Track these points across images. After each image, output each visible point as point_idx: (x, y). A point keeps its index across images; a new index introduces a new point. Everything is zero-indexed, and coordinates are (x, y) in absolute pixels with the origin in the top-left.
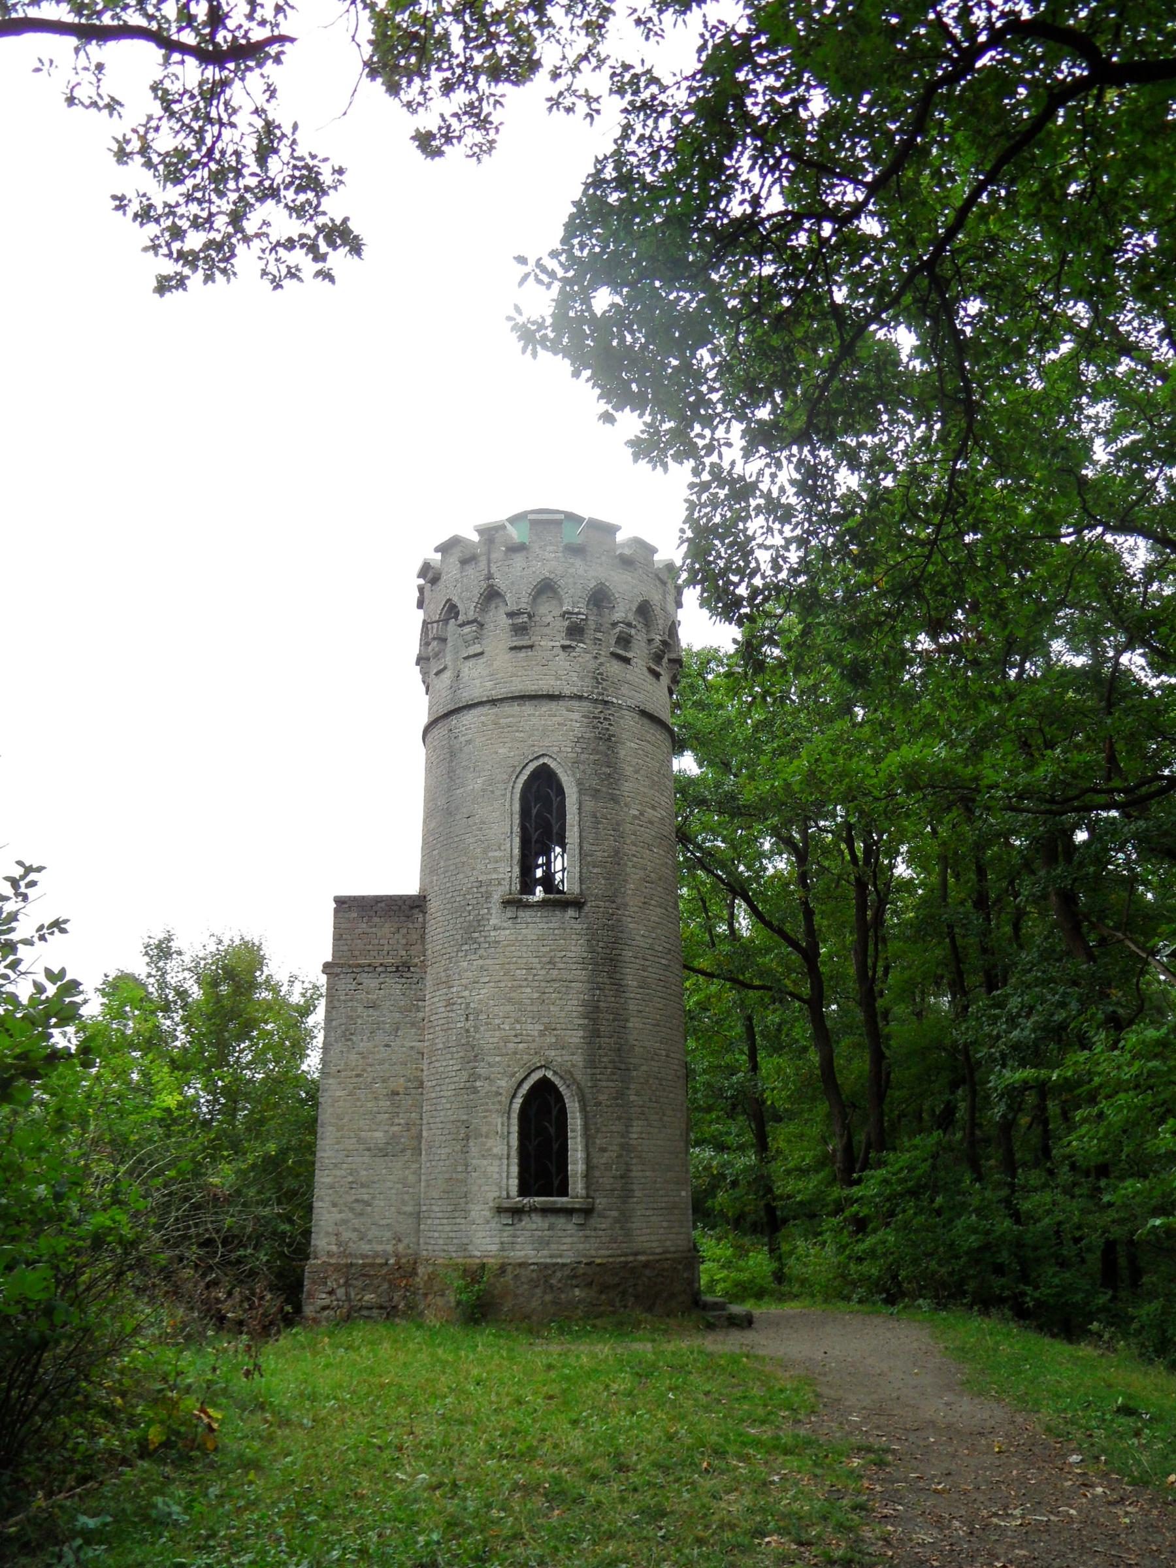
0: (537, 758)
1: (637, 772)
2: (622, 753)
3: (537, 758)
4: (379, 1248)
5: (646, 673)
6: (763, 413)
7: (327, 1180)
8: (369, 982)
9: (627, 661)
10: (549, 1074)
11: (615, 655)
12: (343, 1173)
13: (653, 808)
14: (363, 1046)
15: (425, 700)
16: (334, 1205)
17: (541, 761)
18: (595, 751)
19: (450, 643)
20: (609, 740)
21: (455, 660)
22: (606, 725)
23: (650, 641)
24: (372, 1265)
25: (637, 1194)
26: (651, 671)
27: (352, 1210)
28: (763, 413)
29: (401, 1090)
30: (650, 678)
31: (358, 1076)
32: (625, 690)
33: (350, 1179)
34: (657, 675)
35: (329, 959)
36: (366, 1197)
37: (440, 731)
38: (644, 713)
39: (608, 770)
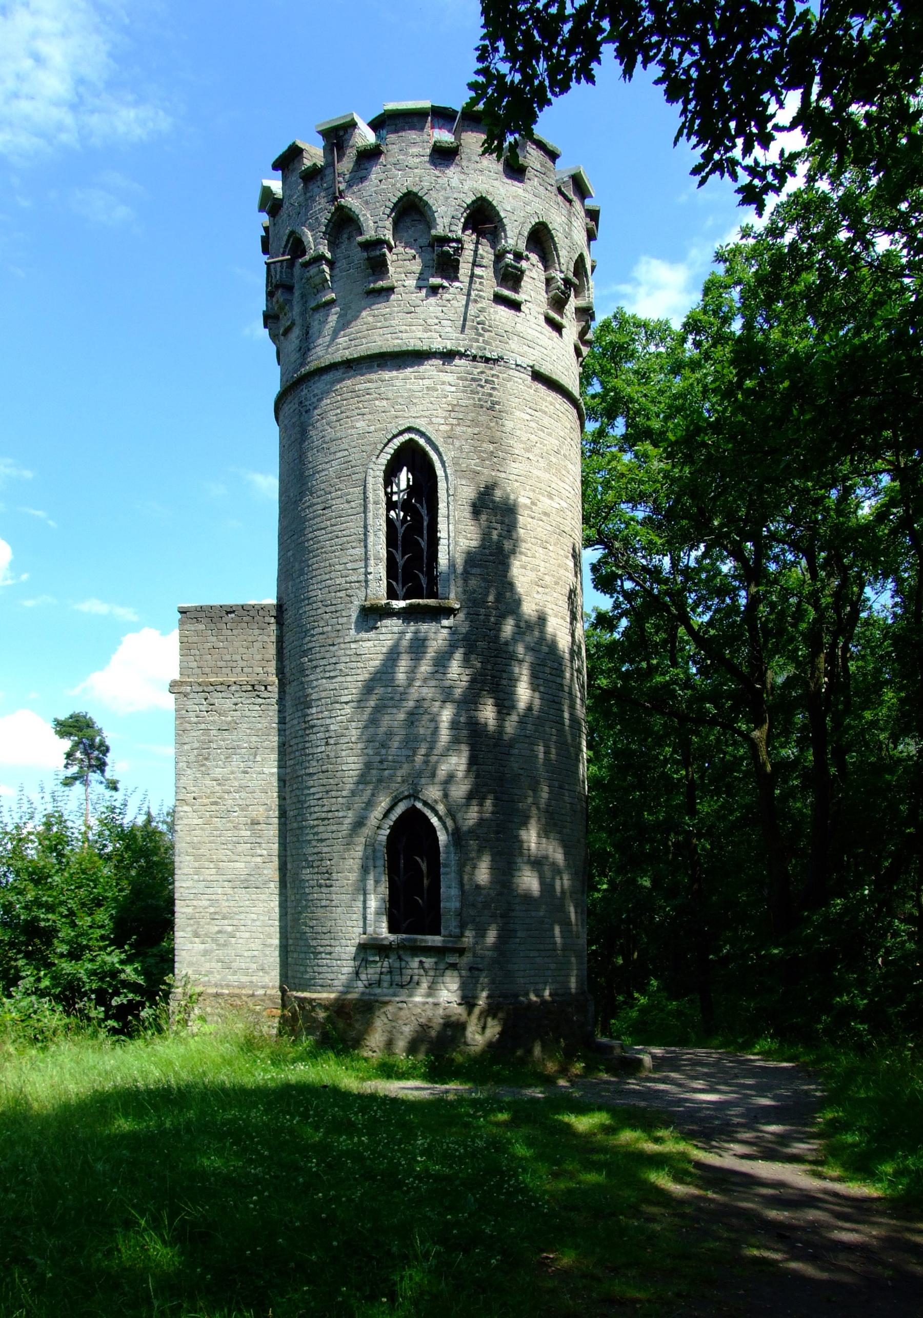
0: (401, 433)
1: (528, 450)
2: (509, 425)
3: (401, 433)
4: (244, 979)
5: (543, 323)
6: (903, 694)
7: (189, 910)
8: (223, 702)
9: (515, 306)
10: (419, 805)
11: (499, 299)
12: (206, 903)
13: (550, 496)
14: (218, 772)
15: (277, 370)
16: (196, 935)
17: (407, 436)
18: (475, 423)
19: (297, 293)
20: (491, 409)
21: (303, 313)
22: (487, 389)
23: (549, 281)
24: (239, 996)
25: (519, 934)
26: (550, 321)
27: (214, 940)
28: (903, 694)
29: (261, 820)
30: (548, 330)
31: (216, 803)
32: (514, 344)
33: (212, 910)
34: (558, 328)
35: (177, 677)
36: (230, 929)
37: (287, 409)
38: (538, 376)
39: (491, 447)
